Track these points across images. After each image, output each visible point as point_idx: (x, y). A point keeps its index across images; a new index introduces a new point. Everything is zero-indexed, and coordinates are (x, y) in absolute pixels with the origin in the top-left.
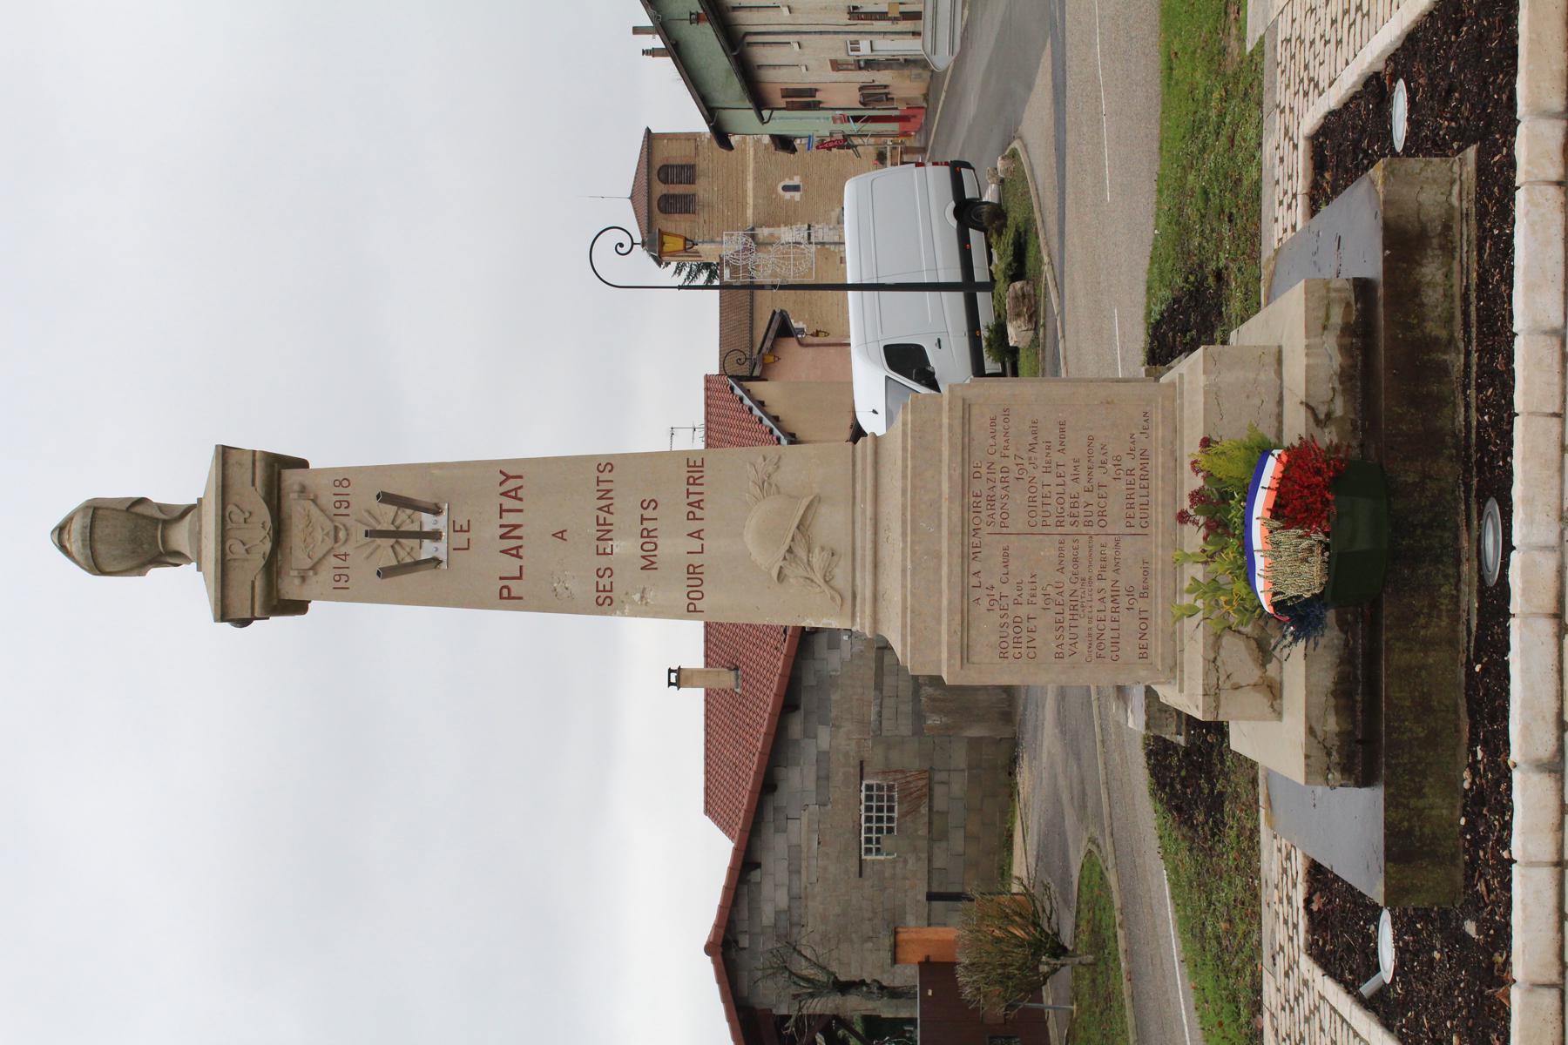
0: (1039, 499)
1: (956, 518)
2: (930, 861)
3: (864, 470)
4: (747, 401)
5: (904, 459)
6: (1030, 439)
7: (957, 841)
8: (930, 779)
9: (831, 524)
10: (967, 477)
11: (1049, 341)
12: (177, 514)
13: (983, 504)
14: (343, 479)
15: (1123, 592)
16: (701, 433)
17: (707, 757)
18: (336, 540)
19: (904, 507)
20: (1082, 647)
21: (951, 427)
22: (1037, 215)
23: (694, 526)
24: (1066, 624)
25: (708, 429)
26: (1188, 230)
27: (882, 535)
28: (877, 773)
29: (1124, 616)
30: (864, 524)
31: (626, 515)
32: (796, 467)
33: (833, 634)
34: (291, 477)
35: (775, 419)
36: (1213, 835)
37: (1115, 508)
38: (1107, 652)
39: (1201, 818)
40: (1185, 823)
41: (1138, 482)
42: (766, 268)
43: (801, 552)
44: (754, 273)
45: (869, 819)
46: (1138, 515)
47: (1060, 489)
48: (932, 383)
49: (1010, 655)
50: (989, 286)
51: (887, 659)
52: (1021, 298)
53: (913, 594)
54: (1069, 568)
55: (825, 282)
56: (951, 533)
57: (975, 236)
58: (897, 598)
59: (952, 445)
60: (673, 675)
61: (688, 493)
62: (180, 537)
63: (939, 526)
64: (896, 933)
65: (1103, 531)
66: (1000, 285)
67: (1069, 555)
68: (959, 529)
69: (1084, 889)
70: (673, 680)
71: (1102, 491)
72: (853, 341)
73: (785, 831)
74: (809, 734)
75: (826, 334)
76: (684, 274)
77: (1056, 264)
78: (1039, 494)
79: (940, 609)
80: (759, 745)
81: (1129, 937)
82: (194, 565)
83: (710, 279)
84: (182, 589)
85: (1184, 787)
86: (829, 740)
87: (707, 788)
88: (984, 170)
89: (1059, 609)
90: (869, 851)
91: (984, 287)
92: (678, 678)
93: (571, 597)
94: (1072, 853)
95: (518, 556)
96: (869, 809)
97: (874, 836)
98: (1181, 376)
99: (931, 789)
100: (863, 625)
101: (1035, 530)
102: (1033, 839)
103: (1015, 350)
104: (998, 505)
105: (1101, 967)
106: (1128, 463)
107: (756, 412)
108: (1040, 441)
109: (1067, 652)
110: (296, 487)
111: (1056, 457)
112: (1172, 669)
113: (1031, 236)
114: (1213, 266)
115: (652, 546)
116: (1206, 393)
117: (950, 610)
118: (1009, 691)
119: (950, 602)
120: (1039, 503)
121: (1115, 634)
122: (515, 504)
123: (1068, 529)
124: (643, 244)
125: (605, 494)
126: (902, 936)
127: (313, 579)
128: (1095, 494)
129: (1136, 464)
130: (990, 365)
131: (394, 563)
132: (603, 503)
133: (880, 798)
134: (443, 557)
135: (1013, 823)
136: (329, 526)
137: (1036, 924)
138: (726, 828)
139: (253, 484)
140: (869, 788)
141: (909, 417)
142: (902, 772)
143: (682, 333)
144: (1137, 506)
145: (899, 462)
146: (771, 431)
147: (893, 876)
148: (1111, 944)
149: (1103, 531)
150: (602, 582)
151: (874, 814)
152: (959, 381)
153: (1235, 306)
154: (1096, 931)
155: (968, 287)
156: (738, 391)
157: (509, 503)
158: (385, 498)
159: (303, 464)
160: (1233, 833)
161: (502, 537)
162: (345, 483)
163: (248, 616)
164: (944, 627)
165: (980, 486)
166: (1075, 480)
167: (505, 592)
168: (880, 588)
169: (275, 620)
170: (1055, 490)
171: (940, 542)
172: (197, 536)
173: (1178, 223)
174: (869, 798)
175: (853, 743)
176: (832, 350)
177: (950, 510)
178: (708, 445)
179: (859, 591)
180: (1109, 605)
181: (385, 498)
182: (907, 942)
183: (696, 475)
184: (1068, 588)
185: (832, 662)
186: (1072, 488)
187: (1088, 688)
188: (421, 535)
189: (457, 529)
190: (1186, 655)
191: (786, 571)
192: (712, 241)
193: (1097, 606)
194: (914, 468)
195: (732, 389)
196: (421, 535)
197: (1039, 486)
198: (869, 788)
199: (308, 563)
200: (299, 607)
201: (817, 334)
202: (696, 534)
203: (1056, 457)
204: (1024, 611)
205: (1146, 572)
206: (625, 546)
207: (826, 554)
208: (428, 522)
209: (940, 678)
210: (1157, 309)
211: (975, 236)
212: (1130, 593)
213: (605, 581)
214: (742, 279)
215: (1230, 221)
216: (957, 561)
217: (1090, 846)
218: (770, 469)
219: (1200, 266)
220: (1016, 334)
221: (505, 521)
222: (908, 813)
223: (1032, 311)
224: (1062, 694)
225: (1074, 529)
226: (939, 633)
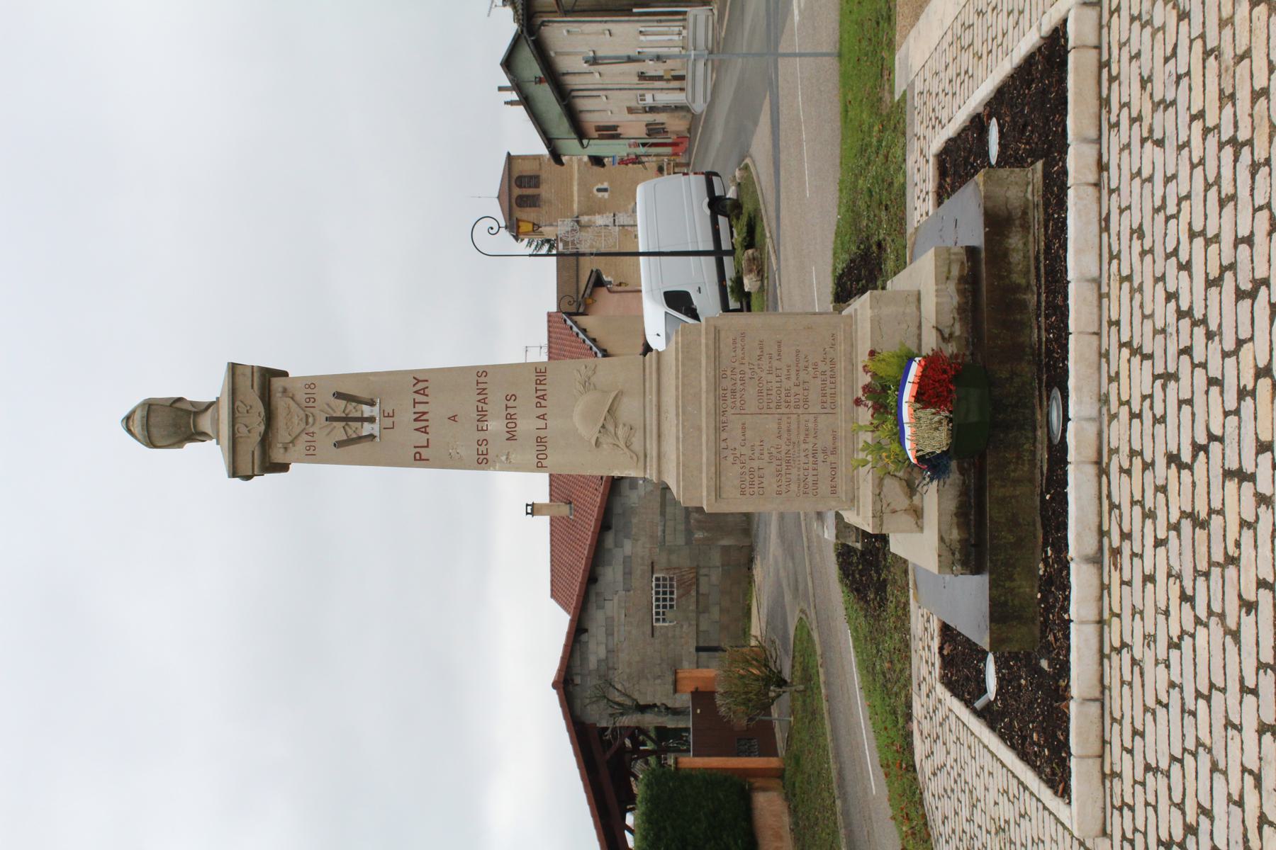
4: (575, 329)
5: (677, 366)
7: (715, 613)
9: (629, 409)
10: (718, 378)
11: (771, 289)
14: (311, 384)
15: (820, 451)
16: (545, 350)
17: (552, 561)
18: (307, 423)
20: (793, 487)
21: (707, 346)
22: (762, 206)
23: (541, 411)
25: (550, 347)
31: (496, 405)
33: (633, 482)
34: (277, 383)
35: (594, 340)
37: (814, 396)
43: (611, 428)
45: (657, 600)
48: (695, 316)
50: (731, 253)
51: (668, 496)
52: (753, 260)
54: (785, 436)
57: (722, 221)
58: (674, 457)
62: (205, 423)
64: (676, 673)
66: (739, 251)
67: (784, 426)
71: (806, 386)
72: (643, 289)
74: (618, 545)
75: (626, 285)
76: (533, 246)
81: (827, 673)
83: (550, 250)
84: (208, 456)
85: (861, 576)
86: (632, 549)
87: (552, 581)
88: (727, 178)
90: (658, 620)
96: (657, 593)
97: (661, 610)
100: (652, 475)
102: (764, 611)
103: (749, 294)
104: (738, 395)
105: (809, 693)
106: (822, 367)
107: (581, 335)
111: (775, 364)
112: (852, 500)
114: (875, 239)
118: (748, 516)
119: (708, 459)
123: (784, 410)
124: (506, 227)
125: (482, 391)
129: (827, 368)
130: (733, 304)
131: (345, 438)
132: (481, 397)
133: (665, 586)
134: (377, 433)
136: (302, 414)
137: (766, 666)
138: (565, 606)
140: (658, 579)
143: (534, 284)
145: (674, 369)
147: (674, 637)
148: (815, 678)
151: (661, 596)
153: (890, 265)
154: (805, 669)
155: (718, 253)
156: (569, 322)
157: (419, 398)
158: (339, 395)
159: (285, 374)
160: (892, 606)
161: (416, 420)
164: (704, 475)
165: (727, 383)
166: (788, 379)
168: (663, 449)
169: (267, 476)
170: (775, 385)
172: (216, 422)
174: (657, 586)
176: (630, 295)
178: (550, 358)
180: (811, 459)
181: (339, 395)
184: (784, 448)
185: (632, 498)
188: (363, 420)
192: (551, 225)
193: (803, 459)
196: (363, 420)
198: (658, 579)
199: (289, 439)
200: (284, 468)
201: (620, 284)
202: (542, 417)
203: (775, 364)
204: (755, 464)
205: (835, 438)
206: (496, 425)
208: (367, 411)
211: (722, 221)
212: (824, 451)
214: (571, 250)
216: (712, 431)
218: (590, 373)
219: (867, 238)
220: (749, 283)
223: (760, 268)
224: (782, 516)
225: (787, 411)
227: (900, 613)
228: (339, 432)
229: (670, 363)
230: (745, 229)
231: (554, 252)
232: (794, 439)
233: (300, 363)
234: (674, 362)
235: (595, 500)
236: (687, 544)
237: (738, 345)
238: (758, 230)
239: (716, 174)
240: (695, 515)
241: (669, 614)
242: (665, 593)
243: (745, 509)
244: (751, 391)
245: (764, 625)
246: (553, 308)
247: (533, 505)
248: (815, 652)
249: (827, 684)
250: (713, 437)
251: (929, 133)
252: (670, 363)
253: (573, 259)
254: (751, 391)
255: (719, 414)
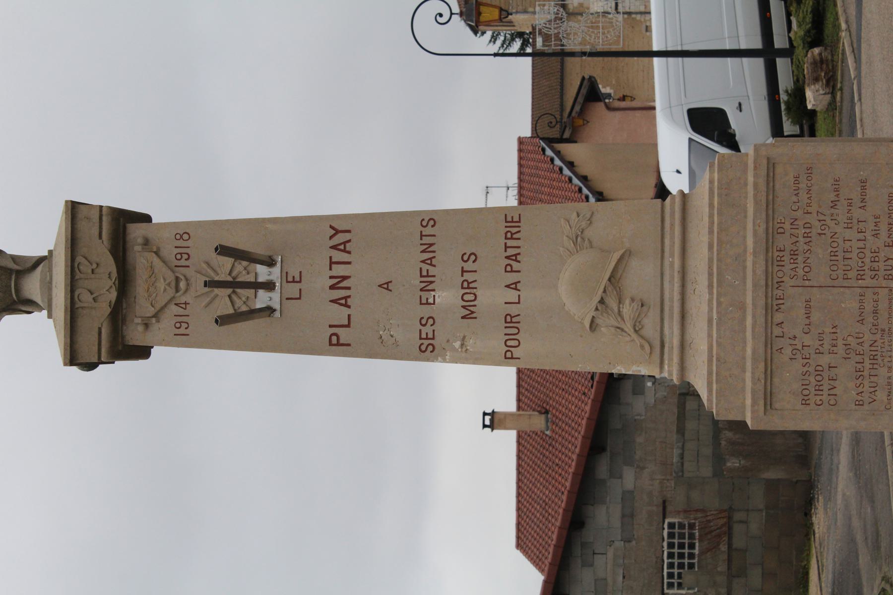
0: (841, 254)
1: (761, 270)
3: (672, 225)
4: (558, 162)
5: (711, 216)
6: (832, 196)
7: (755, 578)
8: (730, 518)
9: (640, 277)
11: (846, 105)
12: (29, 265)
13: (787, 258)
14: (183, 232)
16: (514, 192)
17: (518, 495)
18: (177, 289)
19: (710, 260)
21: (756, 185)
23: (512, 278)
24: (866, 373)
25: (520, 188)
27: (689, 287)
28: (678, 512)
30: (672, 277)
31: (447, 266)
32: (614, 223)
33: (638, 380)
34: (136, 231)
35: (584, 179)
42: (576, 36)
43: (612, 303)
44: (564, 41)
45: (671, 555)
47: (861, 244)
48: (731, 142)
49: (812, 402)
50: (787, 53)
51: (690, 405)
52: (819, 63)
54: (870, 319)
55: (631, 49)
56: (755, 285)
58: (703, 347)
59: (756, 202)
60: (487, 418)
61: (506, 247)
62: (32, 287)
63: (744, 278)
66: (799, 51)
67: (869, 307)
68: (763, 282)
70: (487, 422)
72: (658, 104)
73: (592, 565)
74: (616, 474)
75: (633, 99)
76: (499, 43)
77: (854, 33)
79: (744, 358)
80: (568, 484)
82: (45, 312)
83: (523, 47)
84: (36, 334)
86: (633, 481)
87: (518, 524)
89: (859, 358)
90: (670, 585)
91: (783, 53)
92: (492, 421)
93: (396, 344)
95: (347, 306)
96: (671, 545)
97: (676, 571)
99: (730, 528)
100: (671, 373)
101: (836, 283)
102: (828, 577)
103: (813, 112)
104: (800, 259)
107: (567, 172)
110: (140, 240)
111: (857, 213)
115: (471, 297)
117: (755, 360)
118: (805, 437)
119: (754, 352)
120: (840, 258)
122: (344, 257)
123: (868, 282)
124: (461, 14)
125: (428, 248)
127: (155, 326)
130: (788, 127)
131: (231, 311)
132: (426, 256)
133: (682, 536)
134: (277, 306)
135: (808, 561)
136: (171, 277)
138: (536, 561)
139: (100, 237)
140: (671, 526)
141: (716, 175)
142: (703, 511)
143: (499, 95)
145: (706, 219)
146: (580, 190)
150: (424, 330)
151: (676, 550)
152: (760, 141)
155: (767, 52)
156: (549, 152)
157: (338, 256)
158: (223, 250)
159: (146, 218)
161: (332, 287)
162: (186, 237)
163: (95, 360)
165: (783, 241)
166: (876, 236)
167: (334, 339)
168: (688, 337)
169: (119, 364)
170: (856, 245)
172: (47, 286)
174: (671, 535)
175: (657, 483)
176: (638, 114)
177: (754, 263)
178: (520, 203)
179: (667, 340)
181: (223, 250)
183: (514, 230)
184: (868, 338)
185: (637, 407)
187: (882, 434)
188: (256, 286)
189: (289, 280)
191: (598, 321)
192: (525, 12)
194: (720, 224)
195: (543, 150)
196: (256, 286)
197: (840, 241)
198: (671, 526)
199: (151, 311)
200: (143, 353)
201: (623, 98)
202: (514, 286)
203: (857, 213)
204: (825, 360)
206: (447, 297)
207: (635, 305)
208: (263, 273)
209: (743, 424)
213: (428, 329)
214: (554, 47)
216: (761, 311)
217: (883, 584)
218: (584, 224)
220: (813, 97)
221: (334, 273)
222: (709, 550)
223: (830, 74)
224: (856, 439)
225: (874, 282)
226: (744, 380)
228: (223, 304)
229: (701, 206)
231: (529, 50)
233: (167, 205)
234: (707, 210)
235: (583, 409)
236: (715, 475)
237: (803, 186)
238: (830, 18)
240: (729, 434)
241: (688, 577)
242: (682, 546)
243: (805, 426)
246: (526, 131)
247: (493, 414)
252: (701, 206)
253: (555, 60)
255: (771, 285)
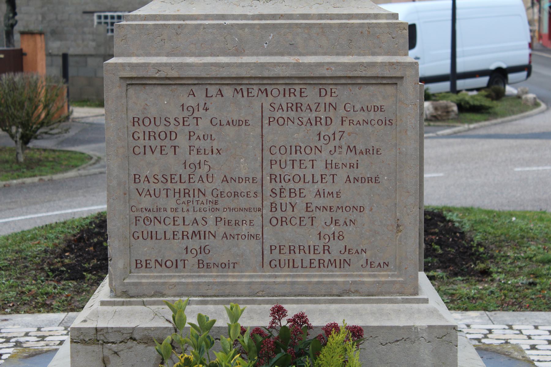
0: (298, 157)
2: (91, 55)
6: (360, 147)
10: (321, 81)
13: (293, 99)
15: (203, 243)
20: (146, 202)
21: (373, 65)
22: (499, 120)
24: (169, 185)
26: (518, 246)
29: (178, 245)
36: (53, 271)
37: (290, 234)
38: (141, 227)
39: (67, 261)
40: (69, 246)
41: (317, 257)
46: (283, 257)
47: (309, 178)
50: (454, 90)
52: (447, 110)
53: (198, 26)
56: (263, 65)
57: (483, 81)
64: (41, 33)
65: (266, 222)
66: (455, 97)
67: (242, 187)
68: (266, 74)
69: (68, 155)
71: (307, 221)
78: (303, 156)
79: (183, 55)
81: (34, 185)
85: (95, 245)
88: (525, 86)
89: (185, 178)
90: (99, 17)
94: (93, 146)
98: (426, 301)
101: (266, 153)
104: (292, 114)
105: (15, 166)
106: (336, 246)
108: (357, 157)
109: (141, 186)
111: (342, 174)
112: (125, 294)
113: (486, 116)
114: (493, 268)
116: (409, 328)
117: (181, 66)
120: (294, 156)
121: (161, 235)
123: (268, 186)
126: (39, 38)
128: (304, 214)
129: (335, 254)
137: (42, 124)
144: (292, 256)
147: (84, 33)
148: (29, 173)
149: (266, 222)
153: (463, 288)
154: (39, 163)
155: (454, 76)
160: (50, 289)
164: (164, 60)
166: (318, 193)
171: (253, 54)
173: (523, 237)
177: (287, 64)
180: (190, 229)
182: (35, 42)
184: (208, 187)
186: (310, 190)
190: (139, 308)
193: (189, 217)
203: (342, 174)
204: (182, 141)
205: (224, 266)
210: (454, 218)
211: (483, 81)
212: (203, 250)
215: (530, 284)
216: (234, 73)
217: (95, 158)
219: (492, 257)
225: (267, 192)
226: (158, 55)
227: (40, 300)
230: (477, 103)
232: (223, 202)
239: (529, 75)
241: (102, 28)
244: (298, 135)
245: (91, 120)
248: (56, 173)
249: (21, 186)
250: (224, 73)
251: (380, 99)
254: (298, 135)
